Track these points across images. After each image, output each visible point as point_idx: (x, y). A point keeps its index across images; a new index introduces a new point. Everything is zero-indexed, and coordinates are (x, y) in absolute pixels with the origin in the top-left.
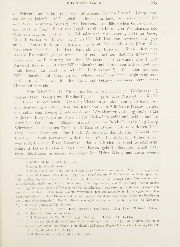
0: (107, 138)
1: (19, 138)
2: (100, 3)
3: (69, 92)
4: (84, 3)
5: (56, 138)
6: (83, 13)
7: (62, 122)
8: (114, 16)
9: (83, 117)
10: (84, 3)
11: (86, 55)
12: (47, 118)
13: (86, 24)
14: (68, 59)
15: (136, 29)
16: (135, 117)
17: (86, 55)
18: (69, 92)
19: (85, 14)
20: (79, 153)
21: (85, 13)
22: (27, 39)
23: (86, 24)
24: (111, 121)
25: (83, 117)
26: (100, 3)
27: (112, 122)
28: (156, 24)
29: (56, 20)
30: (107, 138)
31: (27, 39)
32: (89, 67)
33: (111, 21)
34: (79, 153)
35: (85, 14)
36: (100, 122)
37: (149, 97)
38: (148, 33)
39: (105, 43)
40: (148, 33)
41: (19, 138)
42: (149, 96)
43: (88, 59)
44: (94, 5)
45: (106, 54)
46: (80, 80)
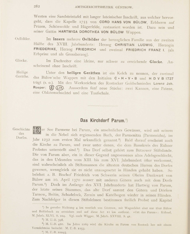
1: (78, 175)
2: (130, 7)
4: (79, 7)
5: (150, 136)
7: (137, 150)
9: (85, 22)
10: (79, 7)
11: (56, 54)
13: (90, 45)
14: (156, 40)
15: (94, 140)
16: (107, 79)
17: (56, 54)
22: (76, 174)
23: (90, 45)
25: (85, 22)
26: (130, 7)
28: (45, 196)
29: (22, 131)
32: (137, 86)
33: (139, 148)
37: (43, 145)
39: (124, 134)
40: (127, 83)
41: (78, 175)
42: (43, 145)
43: (35, 15)
44: (88, 5)
45: (69, 179)
46: (86, 195)
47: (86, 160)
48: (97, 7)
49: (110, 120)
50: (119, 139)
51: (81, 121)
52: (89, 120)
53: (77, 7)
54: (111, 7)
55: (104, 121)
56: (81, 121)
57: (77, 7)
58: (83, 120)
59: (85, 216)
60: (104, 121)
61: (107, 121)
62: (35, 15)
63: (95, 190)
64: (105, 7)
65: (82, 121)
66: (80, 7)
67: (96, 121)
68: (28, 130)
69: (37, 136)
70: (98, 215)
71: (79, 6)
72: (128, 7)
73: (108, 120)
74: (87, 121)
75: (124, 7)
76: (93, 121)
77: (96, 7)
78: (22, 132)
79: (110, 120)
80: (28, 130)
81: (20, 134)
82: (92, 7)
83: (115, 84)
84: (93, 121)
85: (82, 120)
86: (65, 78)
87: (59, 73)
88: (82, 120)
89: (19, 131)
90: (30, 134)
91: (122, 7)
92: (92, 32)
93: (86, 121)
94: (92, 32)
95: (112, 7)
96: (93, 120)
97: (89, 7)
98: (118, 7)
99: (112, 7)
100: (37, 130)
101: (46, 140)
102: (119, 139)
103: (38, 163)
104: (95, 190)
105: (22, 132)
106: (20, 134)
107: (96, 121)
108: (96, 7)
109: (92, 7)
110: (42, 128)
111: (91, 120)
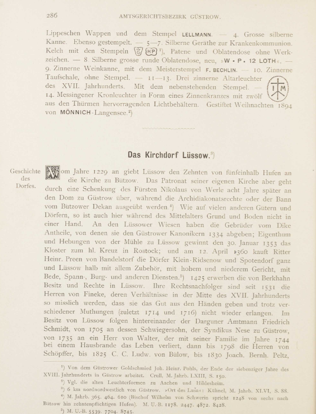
0: (81, 354)
1: (269, 323)
2: (216, 17)
3: (140, 87)
4: (126, 16)
6: (156, 33)
8: (255, 178)
10: (126, 16)
12: (174, 52)
18: (140, 87)
19: (222, 105)
20: (274, 172)
21: (222, 104)
22: (266, 321)
24: (173, 285)
26: (216, 17)
27: (175, 286)
30: (81, 354)
31: (266, 321)
34: (274, 172)
35: (222, 105)
36: (232, 191)
38: (254, 269)
40: (254, 269)
43: (237, 104)
46: (187, 172)
47: (198, 376)
48: (158, 17)
49: (180, 155)
50: (212, 152)
51: (129, 157)
52: (143, 155)
53: (123, 16)
54: (182, 17)
55: (170, 156)
56: (129, 157)
57: (123, 16)
58: (133, 155)
59: (237, 105)
60: (170, 156)
61: (174, 156)
62: (237, 104)
63: (148, 339)
64: (173, 17)
65: (130, 156)
66: (128, 16)
67: (155, 156)
68: (38, 172)
69: (53, 183)
70: (169, 374)
71: (126, 15)
72: (212, 17)
73: (176, 154)
74: (139, 155)
75: (205, 17)
76: (150, 156)
77: (156, 17)
78: (26, 176)
79: (180, 155)
80: (38, 172)
81: (24, 179)
82: (149, 16)
83: (149, 251)
84: (150, 156)
85: (131, 155)
86: (87, 70)
87: (182, 322)
88: (131, 155)
89: (21, 175)
90: (40, 180)
91: (202, 17)
92: (271, 61)
93: (137, 156)
94: (271, 61)
95: (184, 17)
96: (149, 155)
97: (143, 16)
98: (194, 16)
99: (184, 17)
100: (53, 173)
101: (201, 278)
102: (212, 152)
103: (78, 222)
104: (148, 339)
105: (26, 176)
106: (24, 179)
107: (155, 156)
108: (156, 17)
109: (149, 16)
110: (61, 169)
111: (147, 155)
